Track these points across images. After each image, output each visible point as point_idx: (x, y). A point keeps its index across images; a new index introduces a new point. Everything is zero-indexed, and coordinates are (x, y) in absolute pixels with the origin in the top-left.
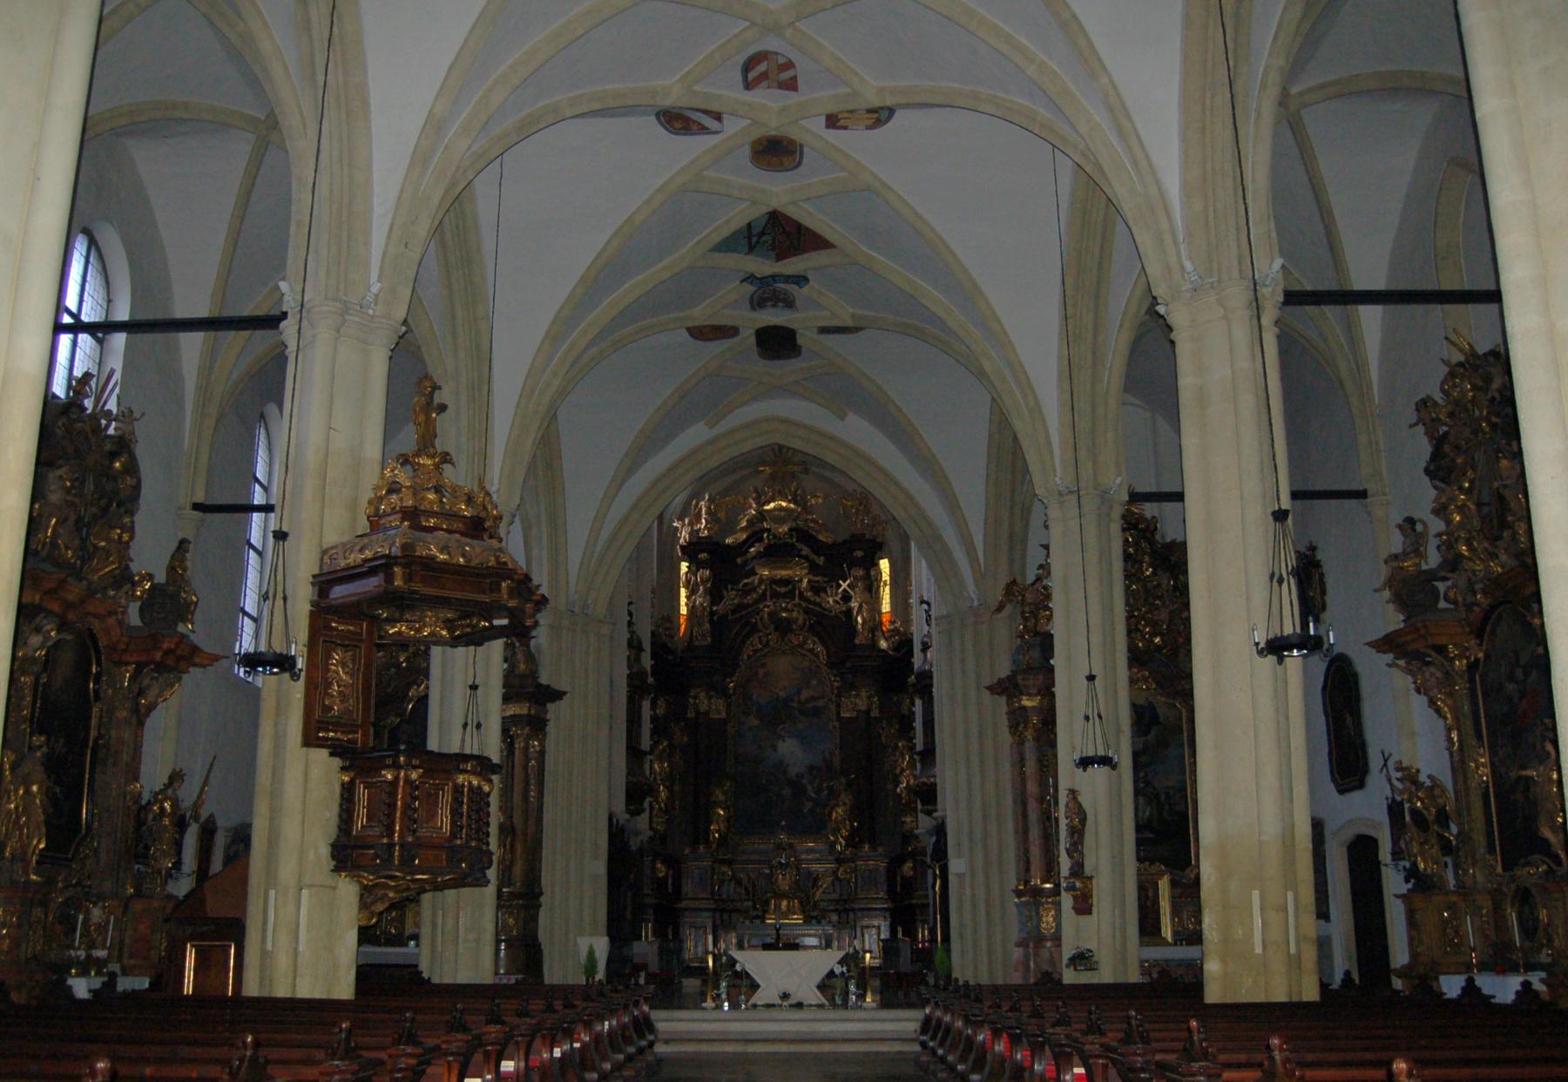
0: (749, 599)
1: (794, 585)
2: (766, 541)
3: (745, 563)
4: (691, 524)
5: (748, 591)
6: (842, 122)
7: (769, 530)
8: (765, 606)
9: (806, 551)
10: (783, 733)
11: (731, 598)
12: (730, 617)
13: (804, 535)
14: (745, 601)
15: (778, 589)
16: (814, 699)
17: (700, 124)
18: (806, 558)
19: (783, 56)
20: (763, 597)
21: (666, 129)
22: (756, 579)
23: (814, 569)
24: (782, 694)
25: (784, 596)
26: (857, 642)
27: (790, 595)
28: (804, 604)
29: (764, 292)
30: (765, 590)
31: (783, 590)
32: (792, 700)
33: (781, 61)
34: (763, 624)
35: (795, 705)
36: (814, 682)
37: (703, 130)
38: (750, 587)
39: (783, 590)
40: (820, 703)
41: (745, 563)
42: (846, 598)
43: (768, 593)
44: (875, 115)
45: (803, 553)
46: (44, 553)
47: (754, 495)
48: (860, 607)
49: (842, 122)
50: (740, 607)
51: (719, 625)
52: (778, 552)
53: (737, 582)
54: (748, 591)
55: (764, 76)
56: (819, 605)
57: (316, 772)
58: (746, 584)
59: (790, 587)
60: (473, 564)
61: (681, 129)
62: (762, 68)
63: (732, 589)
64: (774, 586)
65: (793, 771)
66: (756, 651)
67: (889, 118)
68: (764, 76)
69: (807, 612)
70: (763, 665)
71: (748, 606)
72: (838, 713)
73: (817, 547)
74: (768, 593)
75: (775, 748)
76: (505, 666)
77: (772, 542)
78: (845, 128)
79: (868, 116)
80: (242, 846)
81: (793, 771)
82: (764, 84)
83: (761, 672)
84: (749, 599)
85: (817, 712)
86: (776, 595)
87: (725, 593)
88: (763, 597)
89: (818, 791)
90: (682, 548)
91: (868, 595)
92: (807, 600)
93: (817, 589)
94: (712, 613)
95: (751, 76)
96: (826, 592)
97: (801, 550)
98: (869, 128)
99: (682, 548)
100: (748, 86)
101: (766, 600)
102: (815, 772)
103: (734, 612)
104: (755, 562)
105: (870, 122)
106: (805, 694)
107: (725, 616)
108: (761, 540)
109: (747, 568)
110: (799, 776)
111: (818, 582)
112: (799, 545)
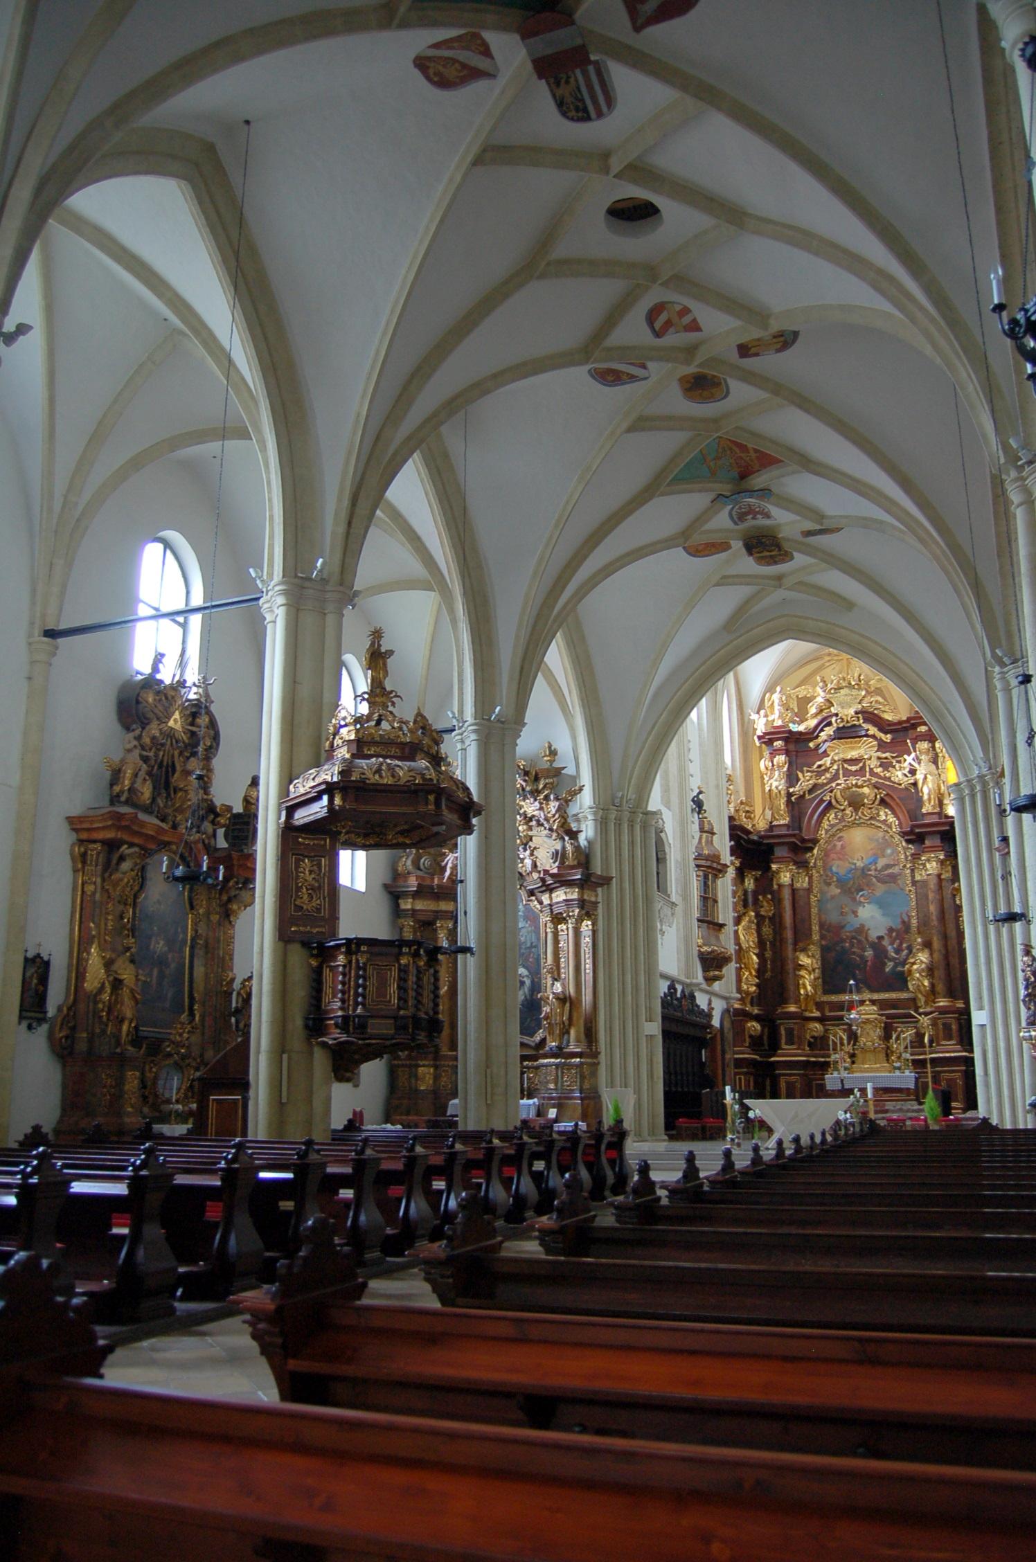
0: (822, 780)
1: (864, 764)
2: (835, 725)
3: (817, 747)
4: (766, 716)
5: (821, 772)
6: (753, 351)
7: (837, 715)
8: (838, 785)
9: (873, 730)
10: (862, 899)
11: (805, 781)
12: (807, 797)
13: (871, 717)
14: (820, 781)
15: (850, 768)
16: (888, 866)
17: (628, 374)
18: (874, 736)
19: (679, 303)
20: (835, 777)
21: (600, 383)
22: (828, 761)
23: (882, 746)
24: (860, 864)
25: (855, 773)
26: (924, 811)
27: (861, 772)
28: (874, 780)
29: (740, 508)
30: (838, 770)
31: (854, 768)
32: (870, 870)
33: (678, 308)
34: (837, 802)
35: (872, 873)
36: (889, 851)
37: (633, 378)
38: (823, 768)
39: (854, 768)
40: (896, 870)
41: (817, 747)
42: (913, 772)
43: (841, 772)
44: (782, 339)
45: (870, 733)
46: (123, 799)
47: (821, 684)
48: (925, 778)
49: (753, 351)
50: (815, 787)
51: (796, 805)
52: (846, 733)
53: (810, 765)
54: (821, 772)
55: (668, 324)
56: (889, 779)
57: (720, 917)
58: (820, 766)
59: (861, 764)
60: (402, 782)
61: (613, 381)
62: (663, 318)
63: (808, 771)
64: (846, 766)
65: (873, 935)
66: (832, 826)
67: (794, 341)
68: (668, 324)
69: (876, 786)
70: (840, 839)
71: (824, 785)
72: (913, 877)
73: (882, 725)
74: (841, 772)
75: (855, 913)
76: (733, 843)
77: (841, 725)
78: (757, 355)
79: (775, 340)
80: (921, 929)
81: (873, 935)
82: (672, 330)
83: (839, 844)
84: (822, 780)
85: (893, 878)
86: (847, 774)
87: (800, 775)
88: (835, 777)
89: (898, 951)
90: (759, 738)
91: (933, 766)
92: (876, 775)
93: (886, 765)
94: (789, 795)
95: (658, 325)
96: (894, 767)
97: (868, 730)
98: (778, 351)
99: (759, 738)
100: (658, 335)
101: (839, 779)
102: (894, 934)
103: (811, 791)
104: (827, 744)
105: (778, 346)
106: (881, 862)
107: (802, 797)
108: (830, 724)
109: (821, 751)
110: (880, 938)
111: (886, 758)
112: (865, 726)
